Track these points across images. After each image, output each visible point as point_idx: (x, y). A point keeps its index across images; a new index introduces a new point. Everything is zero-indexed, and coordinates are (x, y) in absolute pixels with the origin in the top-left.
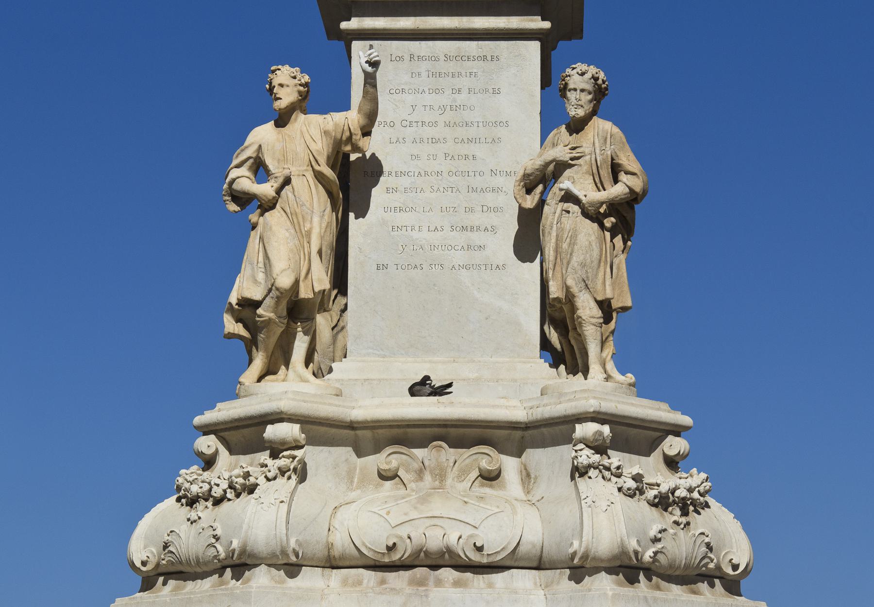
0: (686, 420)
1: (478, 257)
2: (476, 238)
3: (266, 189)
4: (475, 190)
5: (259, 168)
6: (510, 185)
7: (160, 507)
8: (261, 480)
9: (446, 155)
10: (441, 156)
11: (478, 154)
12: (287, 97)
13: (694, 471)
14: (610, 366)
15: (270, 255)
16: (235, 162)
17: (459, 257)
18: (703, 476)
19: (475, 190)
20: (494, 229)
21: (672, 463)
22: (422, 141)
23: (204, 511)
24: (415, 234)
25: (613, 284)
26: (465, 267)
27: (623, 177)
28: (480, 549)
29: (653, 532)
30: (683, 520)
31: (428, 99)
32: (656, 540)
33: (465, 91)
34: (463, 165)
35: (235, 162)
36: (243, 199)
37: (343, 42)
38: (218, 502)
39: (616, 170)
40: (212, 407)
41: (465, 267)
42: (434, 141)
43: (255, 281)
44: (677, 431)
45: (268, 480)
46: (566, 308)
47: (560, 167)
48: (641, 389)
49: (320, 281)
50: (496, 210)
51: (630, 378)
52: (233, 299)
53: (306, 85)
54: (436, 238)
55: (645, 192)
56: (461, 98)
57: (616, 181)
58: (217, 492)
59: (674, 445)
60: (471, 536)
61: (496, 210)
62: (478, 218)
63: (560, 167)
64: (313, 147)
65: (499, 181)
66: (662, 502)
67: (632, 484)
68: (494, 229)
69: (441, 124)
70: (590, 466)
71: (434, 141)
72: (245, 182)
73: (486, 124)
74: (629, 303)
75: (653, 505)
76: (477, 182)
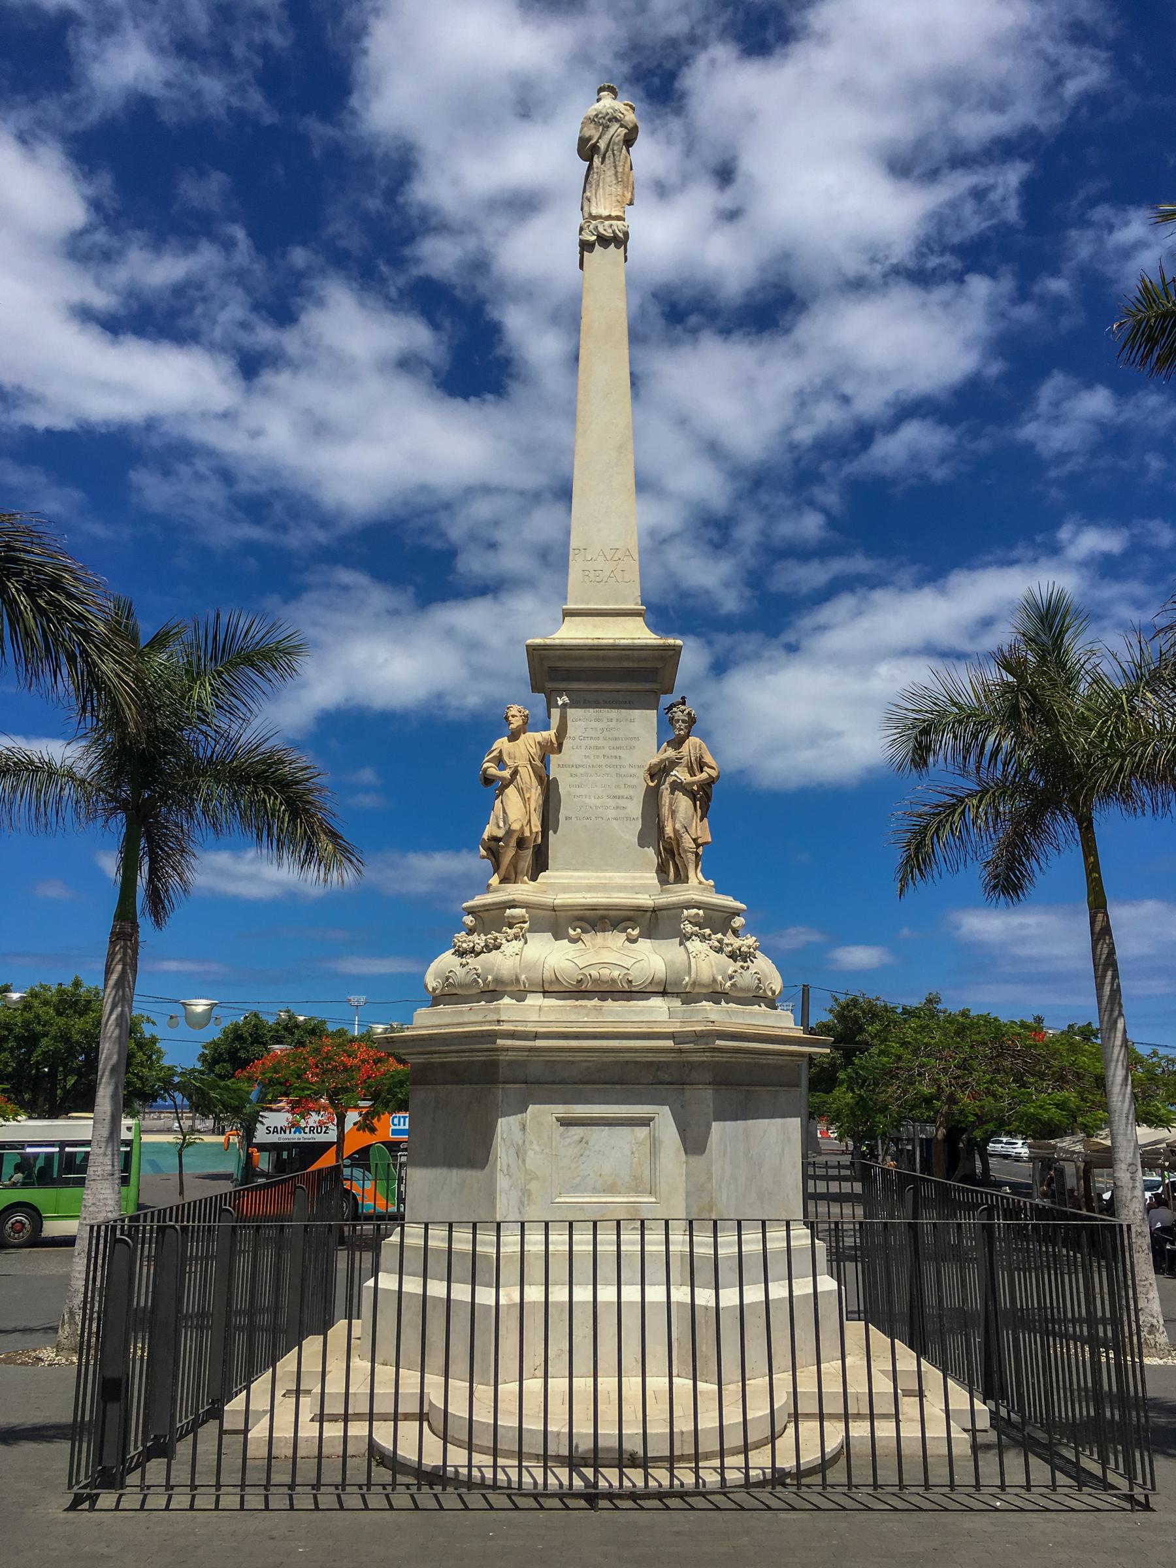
0: (743, 906)
1: (622, 813)
2: (621, 802)
3: (506, 774)
4: (620, 775)
5: (500, 762)
6: (642, 774)
7: (443, 955)
8: (504, 941)
9: (604, 756)
10: (601, 756)
11: (622, 756)
12: (516, 723)
13: (749, 935)
14: (700, 875)
15: (507, 811)
16: (486, 759)
17: (611, 813)
18: (754, 938)
19: (620, 775)
20: (631, 798)
21: (736, 933)
22: (590, 748)
23: (469, 959)
24: (587, 800)
25: (701, 829)
26: (616, 819)
27: (706, 769)
28: (630, 982)
29: (730, 972)
30: (746, 964)
31: (594, 724)
32: (731, 978)
33: (614, 721)
34: (614, 762)
35: (486, 759)
36: (488, 780)
37: (667, 1108)
38: (478, 954)
39: (702, 766)
40: (472, 898)
41: (616, 819)
42: (597, 748)
43: (499, 827)
44: (736, 913)
45: (508, 941)
46: (674, 843)
47: (673, 763)
48: (719, 890)
49: (536, 826)
50: (633, 787)
51: (711, 882)
52: (485, 836)
53: (526, 716)
54: (598, 802)
55: (718, 777)
56: (612, 725)
57: (702, 772)
58: (478, 948)
59: (738, 922)
60: (626, 974)
61: (633, 787)
62: (622, 792)
63: (673, 763)
64: (530, 749)
65: (634, 771)
66: (733, 956)
67: (717, 944)
68: (631, 798)
69: (601, 738)
70: (692, 934)
71: (597, 748)
72: (493, 771)
73: (626, 739)
74: (710, 840)
75: (730, 957)
76: (623, 771)
